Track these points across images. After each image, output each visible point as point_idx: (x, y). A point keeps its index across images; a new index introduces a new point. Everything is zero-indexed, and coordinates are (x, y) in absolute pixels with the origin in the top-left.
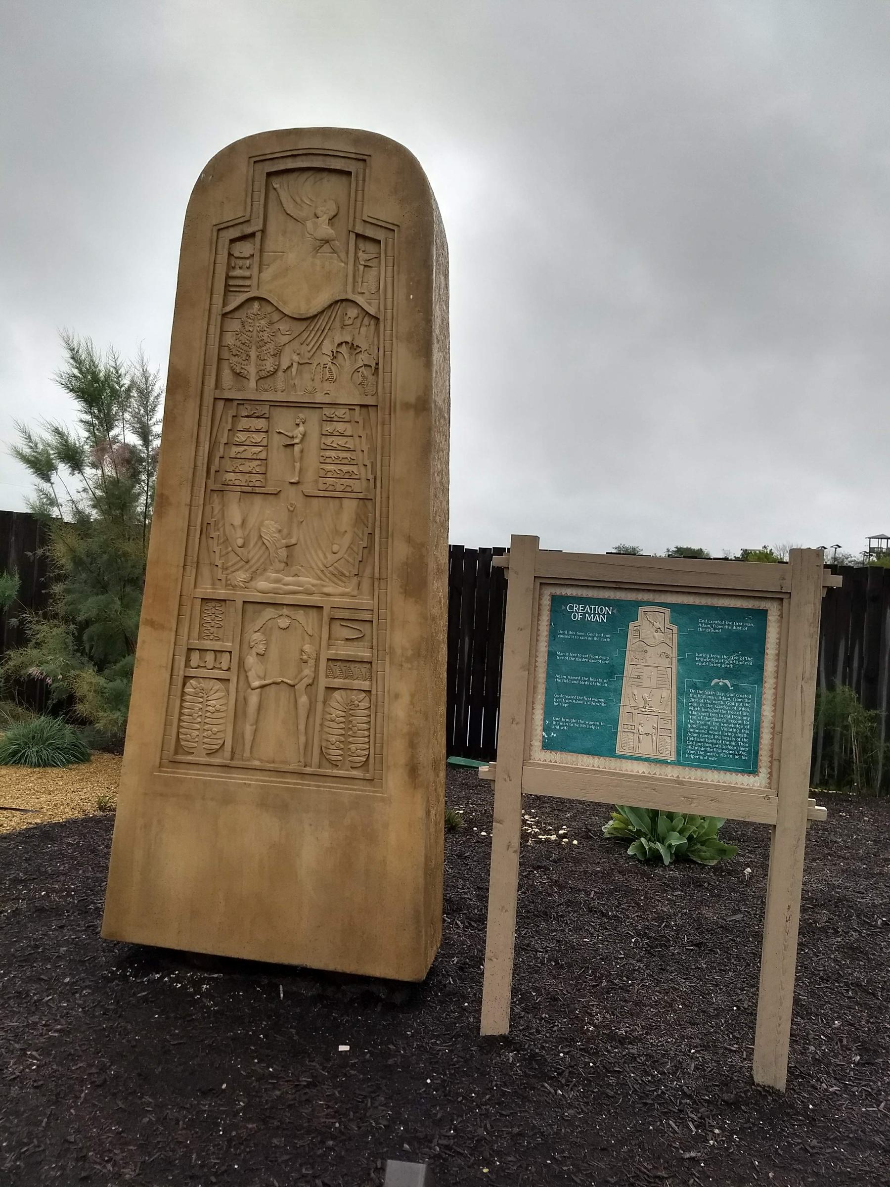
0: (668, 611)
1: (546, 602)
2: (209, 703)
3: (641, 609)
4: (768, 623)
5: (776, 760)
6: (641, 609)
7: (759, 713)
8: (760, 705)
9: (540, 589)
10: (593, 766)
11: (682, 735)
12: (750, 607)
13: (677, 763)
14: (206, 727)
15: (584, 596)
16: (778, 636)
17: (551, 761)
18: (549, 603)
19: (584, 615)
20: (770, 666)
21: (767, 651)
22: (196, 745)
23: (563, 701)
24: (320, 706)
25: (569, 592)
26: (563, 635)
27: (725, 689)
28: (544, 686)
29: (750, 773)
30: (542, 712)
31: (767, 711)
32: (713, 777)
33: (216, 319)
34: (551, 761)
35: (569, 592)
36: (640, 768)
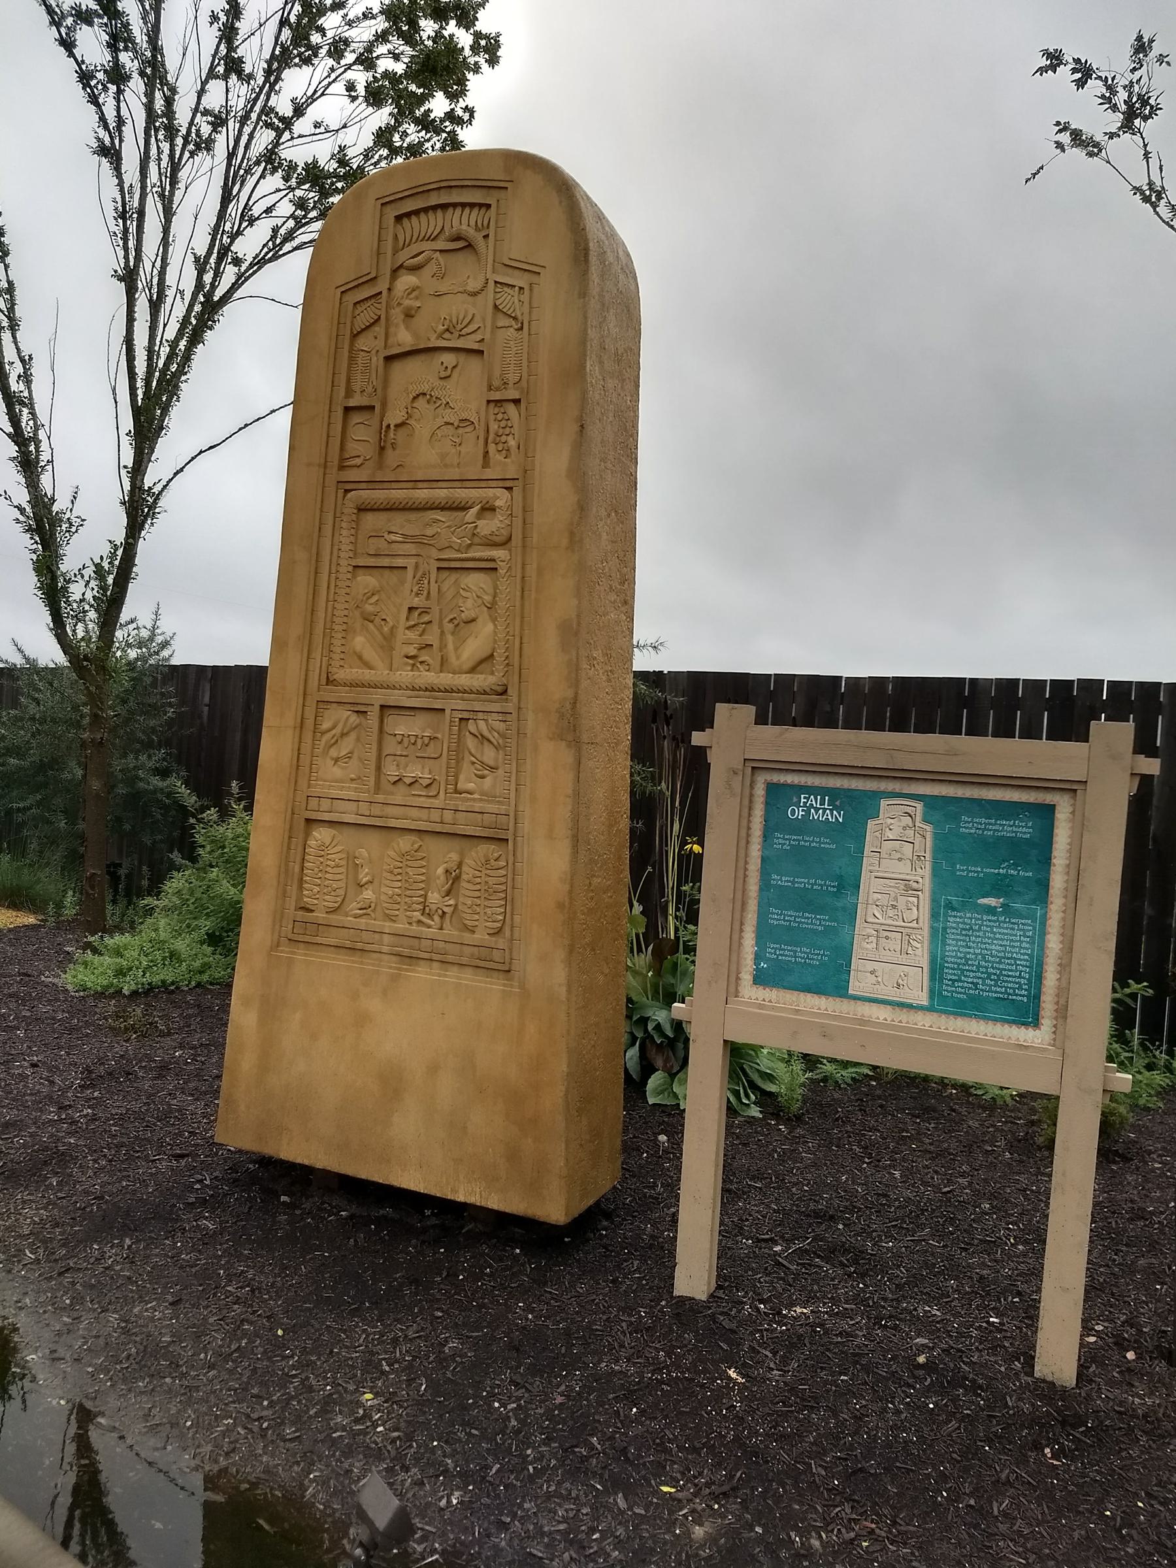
0: (919, 806)
1: (760, 791)
2: (329, 857)
3: (884, 803)
4: (1056, 823)
5: (1062, 1013)
6: (884, 803)
7: (1042, 947)
8: (1043, 933)
9: (753, 774)
10: (819, 1009)
11: (936, 972)
12: (1032, 800)
13: (930, 1009)
14: (327, 882)
15: (809, 784)
16: (1069, 840)
17: (764, 1000)
18: (763, 793)
19: (808, 812)
20: (1058, 880)
21: (1054, 861)
22: (316, 902)
23: (776, 918)
24: (153, 140)
25: (790, 779)
26: (782, 841)
27: (991, 910)
28: (756, 902)
29: (1026, 1024)
30: (753, 935)
31: (1053, 943)
32: (976, 1028)
33: (339, 414)
34: (764, 1000)
35: (790, 779)
36: (881, 1014)
